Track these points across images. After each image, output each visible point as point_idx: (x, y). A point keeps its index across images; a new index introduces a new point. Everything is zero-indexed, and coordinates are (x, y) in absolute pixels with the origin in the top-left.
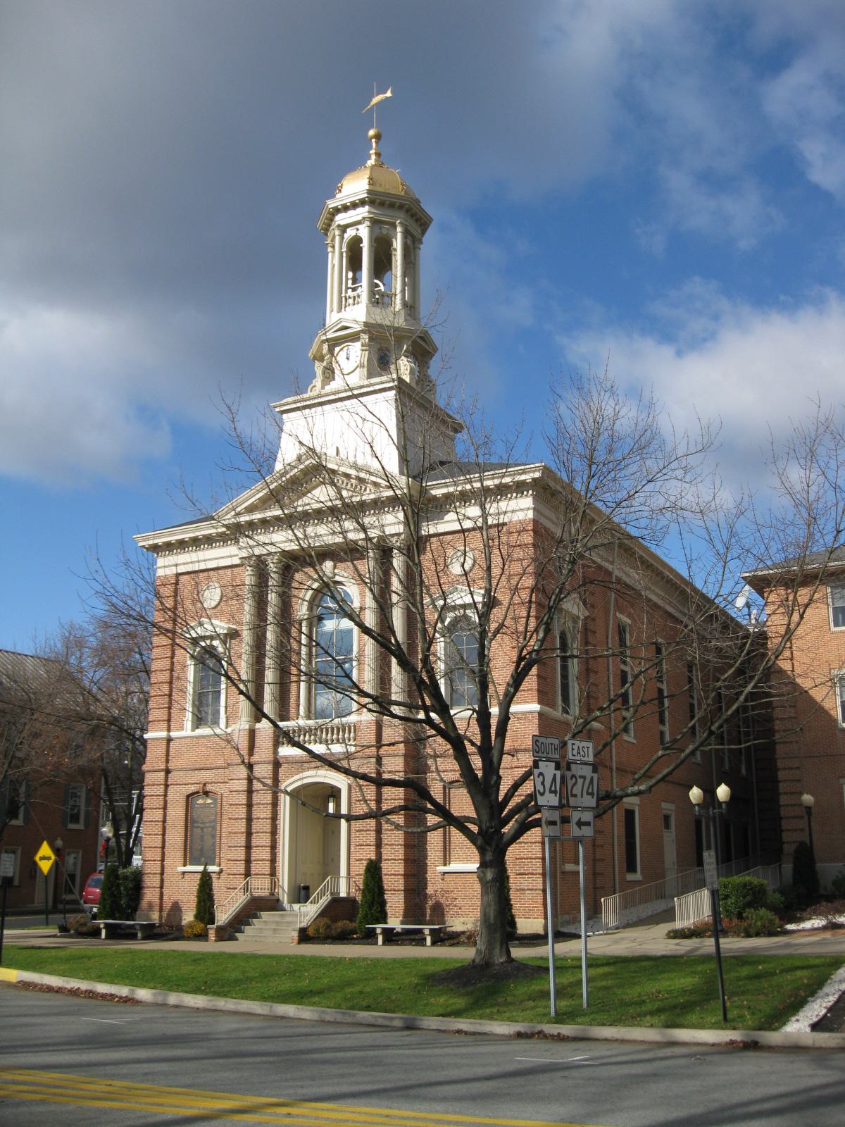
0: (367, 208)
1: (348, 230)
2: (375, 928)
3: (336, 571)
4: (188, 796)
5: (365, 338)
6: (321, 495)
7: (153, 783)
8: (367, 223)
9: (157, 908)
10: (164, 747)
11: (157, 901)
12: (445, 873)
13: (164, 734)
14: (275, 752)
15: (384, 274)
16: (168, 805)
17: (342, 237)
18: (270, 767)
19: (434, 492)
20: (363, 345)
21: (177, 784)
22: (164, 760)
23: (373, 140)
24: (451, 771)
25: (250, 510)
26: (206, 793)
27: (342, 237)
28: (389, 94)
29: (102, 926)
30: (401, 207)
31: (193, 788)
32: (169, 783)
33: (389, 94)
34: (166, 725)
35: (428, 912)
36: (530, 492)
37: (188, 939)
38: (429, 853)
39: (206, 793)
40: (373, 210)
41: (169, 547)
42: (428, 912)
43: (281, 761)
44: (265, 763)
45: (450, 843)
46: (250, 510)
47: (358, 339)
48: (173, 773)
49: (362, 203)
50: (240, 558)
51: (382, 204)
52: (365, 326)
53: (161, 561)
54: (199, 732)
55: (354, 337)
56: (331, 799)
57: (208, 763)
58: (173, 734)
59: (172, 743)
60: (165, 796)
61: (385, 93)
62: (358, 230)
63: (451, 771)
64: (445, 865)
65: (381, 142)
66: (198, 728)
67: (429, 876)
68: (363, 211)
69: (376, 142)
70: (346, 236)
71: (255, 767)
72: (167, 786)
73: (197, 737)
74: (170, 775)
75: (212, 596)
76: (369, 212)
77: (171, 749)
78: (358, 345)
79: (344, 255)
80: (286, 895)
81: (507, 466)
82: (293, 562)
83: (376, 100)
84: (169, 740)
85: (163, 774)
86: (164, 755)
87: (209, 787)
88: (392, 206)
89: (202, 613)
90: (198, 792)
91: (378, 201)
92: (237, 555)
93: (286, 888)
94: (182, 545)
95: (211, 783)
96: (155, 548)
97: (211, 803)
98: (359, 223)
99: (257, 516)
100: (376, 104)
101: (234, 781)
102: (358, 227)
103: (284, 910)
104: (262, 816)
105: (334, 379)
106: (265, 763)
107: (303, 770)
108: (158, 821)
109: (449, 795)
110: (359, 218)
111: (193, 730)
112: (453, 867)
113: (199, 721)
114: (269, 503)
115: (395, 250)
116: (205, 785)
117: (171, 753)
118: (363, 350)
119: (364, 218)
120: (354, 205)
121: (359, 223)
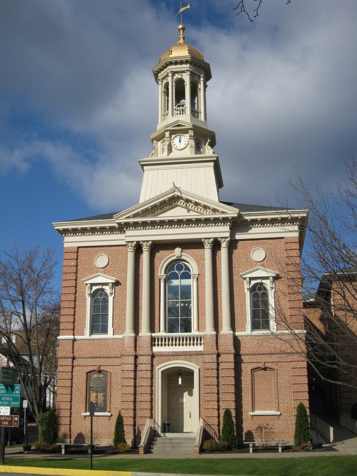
0: (188, 65)
1: (176, 75)
2: (249, 444)
3: (182, 253)
4: (87, 373)
5: (191, 133)
6: (178, 213)
7: (64, 365)
8: (188, 73)
9: (69, 436)
10: (71, 344)
11: (69, 433)
12: (253, 416)
13: (71, 337)
14: (152, 350)
15: (182, 100)
16: (74, 378)
17: (173, 78)
18: (149, 358)
19: (246, 218)
20: (190, 136)
21: (80, 366)
22: (71, 351)
23: (181, 31)
24: (256, 362)
25: (135, 216)
26: (100, 372)
27: (173, 78)
28: (188, 7)
29: (63, 447)
30: (203, 68)
31: (91, 369)
32: (219, 362)
33: (188, 7)
34: (72, 332)
35: (244, 436)
36: (229, 223)
37: (123, 453)
38: (244, 406)
39: (100, 372)
40: (191, 67)
41: (75, 231)
42: (244, 436)
43: (155, 355)
44: (146, 355)
45: (254, 400)
46: (135, 216)
47: (187, 133)
48: (77, 359)
49: (187, 62)
50: (126, 242)
51: (195, 65)
52: (193, 126)
53: (67, 239)
54: (94, 336)
55: (186, 131)
56: (180, 376)
57: (102, 354)
58: (77, 337)
59: (75, 343)
60: (72, 372)
61: (187, 6)
62: (182, 75)
63: (256, 362)
64: (253, 412)
65: (185, 31)
66: (92, 334)
67: (244, 417)
68: (187, 66)
69: (183, 32)
70: (175, 77)
71: (139, 357)
72: (73, 366)
73: (93, 340)
74: (74, 361)
75: (102, 261)
76: (190, 67)
77: (75, 346)
78: (187, 136)
79: (174, 87)
80: (160, 428)
81: (287, 209)
82: (157, 247)
83: (182, 10)
84: (74, 340)
85: (71, 360)
86: (71, 349)
87: (102, 368)
88: (200, 67)
89: (95, 271)
90: (95, 371)
91: (195, 63)
92: (125, 240)
93: (160, 424)
94: (84, 231)
95: (104, 366)
96: (66, 232)
97: (102, 377)
98: (184, 72)
99: (140, 220)
100: (182, 12)
101: (126, 365)
102: (183, 74)
103: (161, 437)
104: (144, 385)
105: (172, 152)
106: (146, 355)
107: (169, 360)
108: (68, 387)
109: (254, 375)
110: (185, 69)
111: (90, 336)
112: (257, 412)
113: (255, 326)
114: (146, 214)
115: (200, 89)
116: (99, 367)
117: (75, 348)
118: (190, 139)
119: (187, 70)
120: (182, 63)
121: (184, 72)
